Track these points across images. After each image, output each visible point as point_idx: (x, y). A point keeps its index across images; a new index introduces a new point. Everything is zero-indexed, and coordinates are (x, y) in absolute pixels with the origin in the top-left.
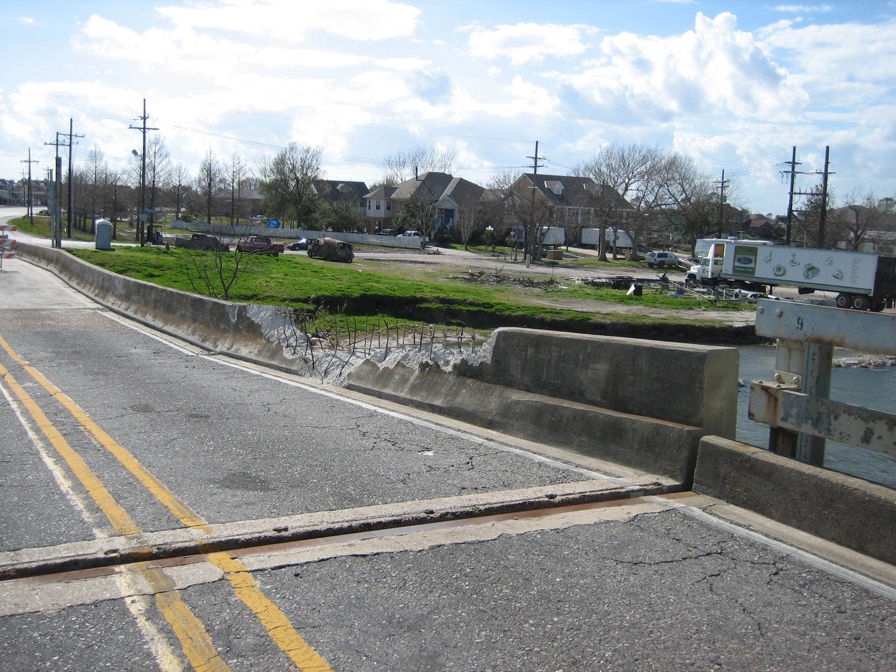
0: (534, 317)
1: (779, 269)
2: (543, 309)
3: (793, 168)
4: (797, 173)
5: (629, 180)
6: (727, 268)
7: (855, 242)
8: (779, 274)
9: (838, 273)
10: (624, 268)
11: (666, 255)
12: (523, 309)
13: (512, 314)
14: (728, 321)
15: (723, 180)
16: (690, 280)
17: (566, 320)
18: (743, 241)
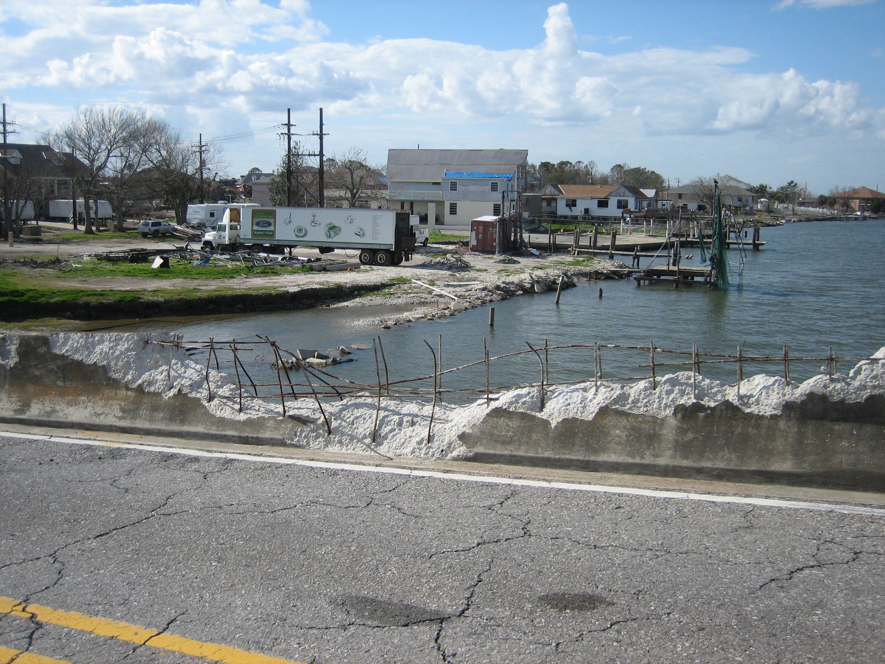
0: (77, 301)
1: (300, 230)
2: (82, 291)
3: (289, 130)
4: (293, 134)
5: (111, 146)
6: (246, 231)
7: (352, 201)
8: (300, 235)
9: (359, 231)
10: (116, 240)
11: (159, 224)
12: (59, 294)
13: (50, 301)
14: (281, 287)
15: (201, 144)
16: (206, 247)
17: (115, 302)
18: (232, 204)
